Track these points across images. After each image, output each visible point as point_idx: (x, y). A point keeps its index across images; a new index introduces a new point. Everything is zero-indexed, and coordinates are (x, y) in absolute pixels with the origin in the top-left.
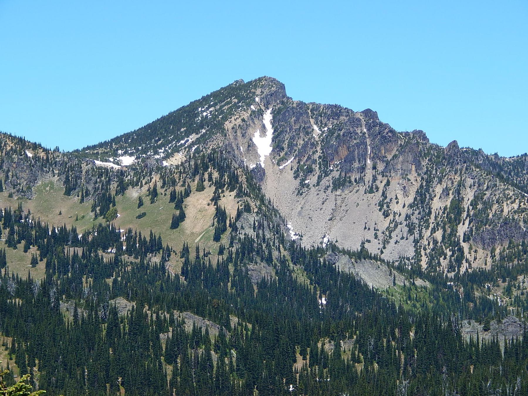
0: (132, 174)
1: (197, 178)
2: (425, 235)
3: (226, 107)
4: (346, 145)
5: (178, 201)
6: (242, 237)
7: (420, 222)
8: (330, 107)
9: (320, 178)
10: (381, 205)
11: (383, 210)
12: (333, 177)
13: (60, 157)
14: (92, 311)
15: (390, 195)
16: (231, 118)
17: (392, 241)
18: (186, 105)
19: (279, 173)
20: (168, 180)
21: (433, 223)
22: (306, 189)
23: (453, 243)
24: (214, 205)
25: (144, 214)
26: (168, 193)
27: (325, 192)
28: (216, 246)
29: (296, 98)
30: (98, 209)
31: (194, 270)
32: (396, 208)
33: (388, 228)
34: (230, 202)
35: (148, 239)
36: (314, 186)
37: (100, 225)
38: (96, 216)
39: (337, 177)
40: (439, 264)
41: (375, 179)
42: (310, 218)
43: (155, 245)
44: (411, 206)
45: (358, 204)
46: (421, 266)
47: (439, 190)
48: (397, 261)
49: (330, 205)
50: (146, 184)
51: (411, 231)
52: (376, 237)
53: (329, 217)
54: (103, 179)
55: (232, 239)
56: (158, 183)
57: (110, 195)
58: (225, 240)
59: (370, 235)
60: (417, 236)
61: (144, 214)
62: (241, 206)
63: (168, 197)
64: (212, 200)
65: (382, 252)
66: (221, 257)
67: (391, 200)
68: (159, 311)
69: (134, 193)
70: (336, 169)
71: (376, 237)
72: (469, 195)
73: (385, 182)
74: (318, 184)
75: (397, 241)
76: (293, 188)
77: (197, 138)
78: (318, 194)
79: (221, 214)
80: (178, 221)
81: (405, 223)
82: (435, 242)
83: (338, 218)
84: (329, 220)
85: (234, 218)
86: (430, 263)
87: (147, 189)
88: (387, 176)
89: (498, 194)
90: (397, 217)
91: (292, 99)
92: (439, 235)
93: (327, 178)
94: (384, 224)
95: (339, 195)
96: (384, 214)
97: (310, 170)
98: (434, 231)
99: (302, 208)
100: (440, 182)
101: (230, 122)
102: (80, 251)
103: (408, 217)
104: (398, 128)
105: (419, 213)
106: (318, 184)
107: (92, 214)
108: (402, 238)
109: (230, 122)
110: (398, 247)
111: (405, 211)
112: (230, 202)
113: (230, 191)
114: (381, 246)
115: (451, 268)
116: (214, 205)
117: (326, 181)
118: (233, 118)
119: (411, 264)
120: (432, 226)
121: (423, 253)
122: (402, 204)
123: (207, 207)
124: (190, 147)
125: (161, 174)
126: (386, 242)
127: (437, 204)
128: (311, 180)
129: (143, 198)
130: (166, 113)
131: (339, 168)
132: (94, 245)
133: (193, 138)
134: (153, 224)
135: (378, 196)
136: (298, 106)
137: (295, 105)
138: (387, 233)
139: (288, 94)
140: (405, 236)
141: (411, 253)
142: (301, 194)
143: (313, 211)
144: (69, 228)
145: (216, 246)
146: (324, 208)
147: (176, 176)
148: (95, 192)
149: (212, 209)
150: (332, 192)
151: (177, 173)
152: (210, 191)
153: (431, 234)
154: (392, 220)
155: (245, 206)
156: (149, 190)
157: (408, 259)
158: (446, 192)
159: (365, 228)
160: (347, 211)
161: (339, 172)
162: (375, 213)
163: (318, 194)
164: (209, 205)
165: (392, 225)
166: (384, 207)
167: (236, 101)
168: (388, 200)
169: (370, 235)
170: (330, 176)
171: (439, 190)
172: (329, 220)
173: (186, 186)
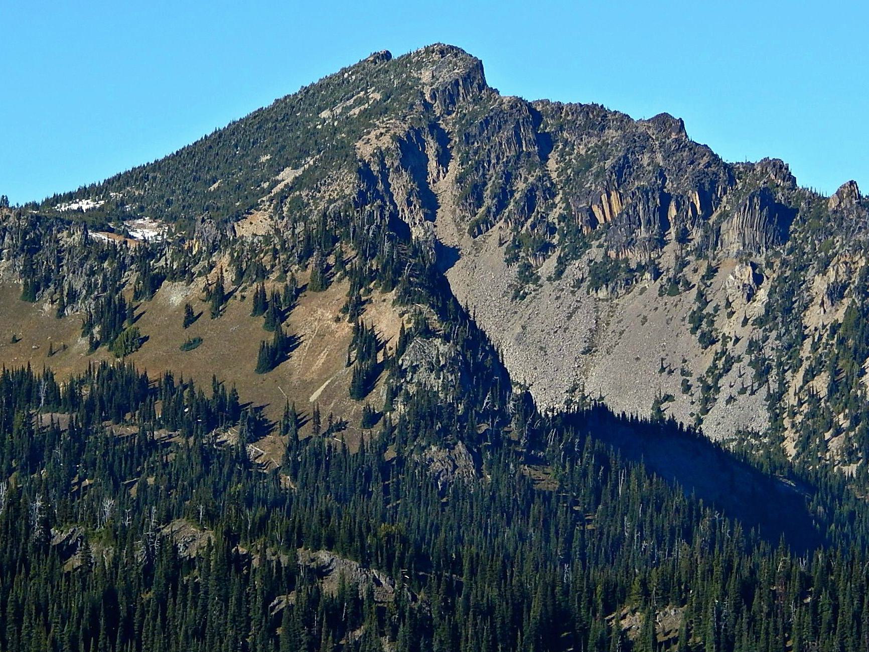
0: (168, 255)
1: (312, 261)
2: (792, 384)
3: (357, 111)
4: (666, 190)
5: (275, 310)
6: (412, 389)
7: (779, 357)
9: (562, 262)
11: (699, 332)
12: (591, 261)
13: (11, 219)
14: (121, 550)
15: (716, 299)
16: (369, 133)
17: (722, 397)
18: (265, 106)
19: (474, 252)
20: (249, 268)
21: (808, 358)
22: (532, 286)
23: (851, 400)
24: (350, 322)
25: (197, 342)
26: (249, 294)
27: (573, 293)
28: (356, 407)
29: (507, 92)
30: (96, 329)
31: (314, 459)
32: (728, 327)
33: (710, 371)
34: (387, 318)
35: (209, 395)
36: (549, 279)
37: (104, 366)
38: (94, 346)
39: (599, 259)
40: (825, 444)
41: (682, 264)
42: (541, 349)
43: (225, 409)
44: (760, 322)
45: (645, 318)
46: (784, 450)
47: (820, 285)
48: (733, 440)
49: (582, 323)
50: (200, 274)
51: (762, 374)
52: (687, 388)
53: (582, 347)
54: (105, 265)
55: (393, 393)
56: (225, 274)
57: (121, 299)
58: (378, 397)
59: (672, 385)
60: (774, 387)
61: (197, 342)
62: (409, 321)
63: (249, 304)
64: (345, 310)
65: (700, 421)
66: (366, 433)
67: (716, 309)
68: (265, 547)
69: (174, 295)
70: (597, 243)
71: (687, 388)
73: (703, 271)
74: (559, 274)
75: (731, 398)
77: (296, 178)
78: (558, 298)
79: (367, 341)
80: (278, 352)
81: (747, 359)
82: (814, 398)
83: (602, 349)
84: (583, 353)
85: (394, 349)
86: (804, 445)
87: (202, 286)
88: (706, 257)
90: (730, 345)
91: (498, 93)
92: (821, 384)
93: (577, 263)
94: (702, 362)
95: (603, 300)
96: (700, 340)
97: (545, 248)
98: (811, 374)
99: (524, 328)
100: (823, 270)
101: (368, 142)
102: (63, 419)
103: (754, 346)
104: (731, 153)
105: (779, 337)
106: (559, 274)
107: (83, 342)
108: (743, 391)
109: (368, 142)
111: (747, 333)
112: (387, 318)
113: (383, 292)
114: (697, 408)
116: (350, 322)
117: (577, 268)
118: (373, 134)
119: (764, 445)
120: (806, 365)
121: (787, 423)
123: (334, 326)
125: (232, 255)
126: (707, 403)
128: (548, 266)
129: (194, 306)
131: (602, 240)
132: (95, 410)
133: (288, 175)
134: (224, 358)
136: (512, 108)
137: (505, 106)
138: (710, 381)
139: (490, 83)
140: (748, 383)
141: (762, 422)
142: (523, 298)
143: (549, 333)
144: (37, 372)
145: (356, 407)
146: (572, 326)
147: (266, 260)
148: (89, 293)
149: (346, 329)
150: (588, 293)
151: (266, 253)
152: (341, 290)
153: (806, 382)
154: (719, 351)
155: (417, 323)
156: (206, 289)
157: (756, 435)
159: (663, 369)
160: (621, 334)
161: (603, 250)
162: (682, 338)
163: (558, 298)
164: (338, 320)
165: (720, 364)
167: (378, 96)
168: (709, 309)
170: (585, 258)
171: (820, 285)
172: (583, 353)
173: (288, 279)
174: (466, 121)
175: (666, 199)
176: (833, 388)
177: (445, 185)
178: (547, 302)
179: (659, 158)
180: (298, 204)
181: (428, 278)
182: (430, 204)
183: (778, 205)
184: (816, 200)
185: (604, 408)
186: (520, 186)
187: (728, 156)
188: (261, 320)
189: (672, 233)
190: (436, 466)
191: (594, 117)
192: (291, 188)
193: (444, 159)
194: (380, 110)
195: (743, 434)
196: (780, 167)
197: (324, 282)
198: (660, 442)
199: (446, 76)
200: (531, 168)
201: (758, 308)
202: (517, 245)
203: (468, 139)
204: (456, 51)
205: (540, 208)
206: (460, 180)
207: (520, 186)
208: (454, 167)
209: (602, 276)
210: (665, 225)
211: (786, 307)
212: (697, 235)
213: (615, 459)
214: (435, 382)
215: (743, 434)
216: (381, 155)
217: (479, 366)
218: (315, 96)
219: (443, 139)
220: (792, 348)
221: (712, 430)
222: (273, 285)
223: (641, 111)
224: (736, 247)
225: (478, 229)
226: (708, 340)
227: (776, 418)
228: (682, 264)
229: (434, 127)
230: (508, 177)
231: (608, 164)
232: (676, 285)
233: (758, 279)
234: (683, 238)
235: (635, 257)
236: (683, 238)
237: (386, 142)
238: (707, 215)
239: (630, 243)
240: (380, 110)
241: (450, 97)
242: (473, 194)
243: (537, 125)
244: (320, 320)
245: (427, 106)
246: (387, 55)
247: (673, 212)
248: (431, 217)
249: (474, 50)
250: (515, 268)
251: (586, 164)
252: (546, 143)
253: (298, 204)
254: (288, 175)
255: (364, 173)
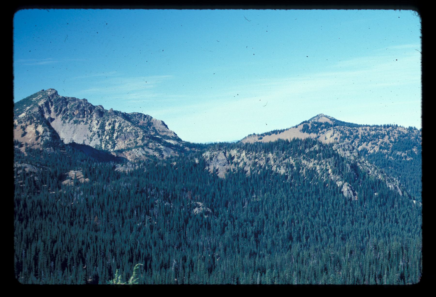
5: (24, 128)
8: (72, 98)
9: (69, 120)
10: (89, 128)
41: (87, 120)
44: (99, 129)
49: (73, 129)
51: (99, 136)
52: (88, 138)
55: (41, 140)
63: (20, 127)
72: (117, 125)
76: (61, 124)
79: (37, 133)
80: (24, 134)
86: (105, 146)
89: (126, 125)
92: (108, 138)
97: (67, 118)
98: (106, 136)
110: (95, 141)
112: (40, 129)
115: (112, 148)
117: (72, 121)
122: (95, 129)
124: (27, 111)
126: (91, 140)
127: (107, 128)
128: (67, 121)
130: (351, 122)
133: (28, 108)
135: (88, 126)
139: (59, 94)
141: (99, 143)
145: (36, 142)
149: (34, 131)
158: (110, 124)
166: (90, 129)
169: (85, 138)
171: (107, 124)
174: (55, 100)
175: (85, 111)
176: (109, 138)
177: (52, 109)
178: (67, 126)
179: (84, 105)
180: (30, 112)
181: (47, 123)
182: (50, 112)
183: (101, 112)
184: (107, 111)
185: (75, 143)
186: (63, 109)
187: (94, 105)
188: (22, 129)
189: (86, 116)
190: (48, 151)
191: (74, 99)
192: (28, 110)
193: (52, 105)
194: (42, 98)
195: (96, 145)
196: (101, 106)
197: (31, 124)
198: (83, 148)
199: (52, 93)
200: (65, 106)
201: (98, 126)
202: (63, 118)
203: (55, 102)
204: (53, 89)
205: (66, 112)
206: (54, 108)
207: (63, 109)
208: (53, 107)
209: (75, 122)
210: (85, 115)
211: (102, 127)
212: (89, 116)
213: (75, 149)
214: (48, 138)
215: (96, 145)
216: (42, 105)
217: (55, 135)
218: (32, 96)
219: (52, 102)
220: (103, 132)
221: (91, 145)
222: (23, 124)
223: (81, 98)
224: (95, 118)
225: (57, 115)
226: (91, 131)
227: (101, 143)
228: (87, 120)
229: (50, 101)
230: (61, 108)
231: (76, 106)
232: (87, 123)
233: (98, 122)
234: (87, 116)
235: (80, 119)
236: (87, 116)
237: (43, 103)
238: (91, 113)
239: (79, 117)
240: (42, 98)
241: (52, 96)
242: (56, 111)
243: (65, 101)
244: (31, 129)
245: (49, 97)
246: (43, 90)
247: (86, 113)
248: (50, 114)
249: (56, 89)
250: (63, 121)
251: (73, 106)
252: (67, 103)
253: (30, 112)
254: (28, 108)
255: (40, 107)
